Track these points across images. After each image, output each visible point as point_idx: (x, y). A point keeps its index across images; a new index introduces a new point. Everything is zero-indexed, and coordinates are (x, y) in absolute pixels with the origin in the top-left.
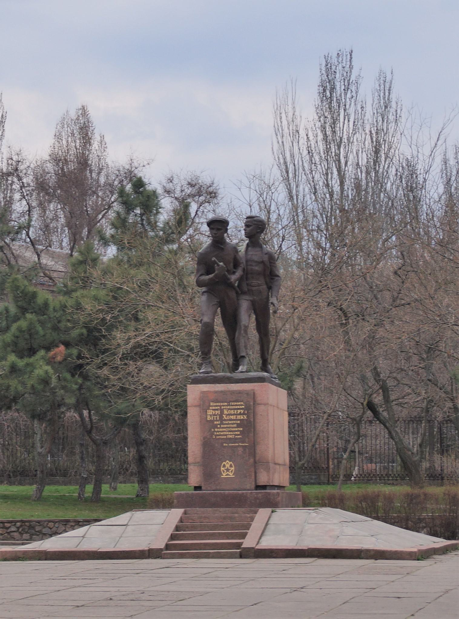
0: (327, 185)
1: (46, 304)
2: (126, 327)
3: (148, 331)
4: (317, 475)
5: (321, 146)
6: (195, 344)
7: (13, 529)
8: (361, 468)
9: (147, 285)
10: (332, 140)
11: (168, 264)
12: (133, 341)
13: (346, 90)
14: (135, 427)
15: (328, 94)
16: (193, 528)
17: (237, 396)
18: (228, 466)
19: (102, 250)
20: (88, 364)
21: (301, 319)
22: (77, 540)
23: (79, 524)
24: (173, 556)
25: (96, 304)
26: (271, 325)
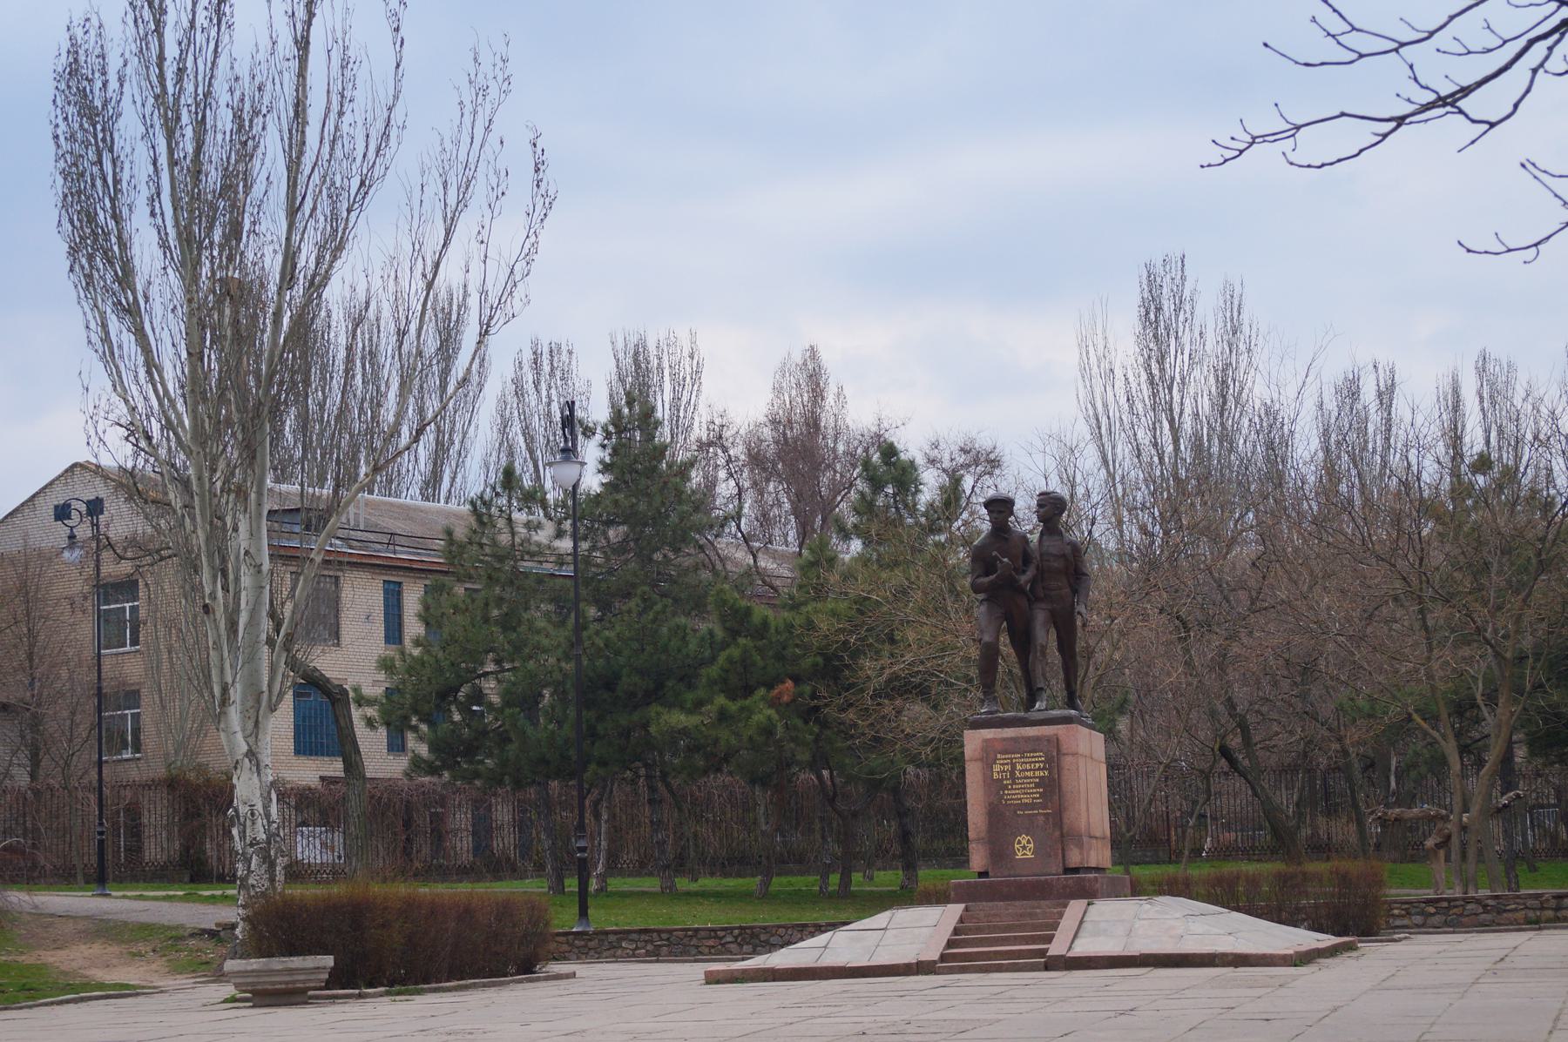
0: (1155, 445)
1: (765, 623)
2: (878, 652)
3: (909, 657)
4: (1154, 851)
5: (1146, 392)
6: (974, 672)
7: (729, 939)
8: (1216, 839)
9: (904, 592)
10: (1159, 381)
11: (934, 563)
12: (887, 671)
13: (1177, 310)
14: (895, 791)
15: (1152, 316)
16: (979, 930)
17: (1034, 744)
18: (1024, 842)
19: (842, 546)
20: (826, 705)
21: (1121, 633)
22: (817, 953)
23: (819, 929)
24: (951, 971)
25: (834, 621)
26: (1080, 645)
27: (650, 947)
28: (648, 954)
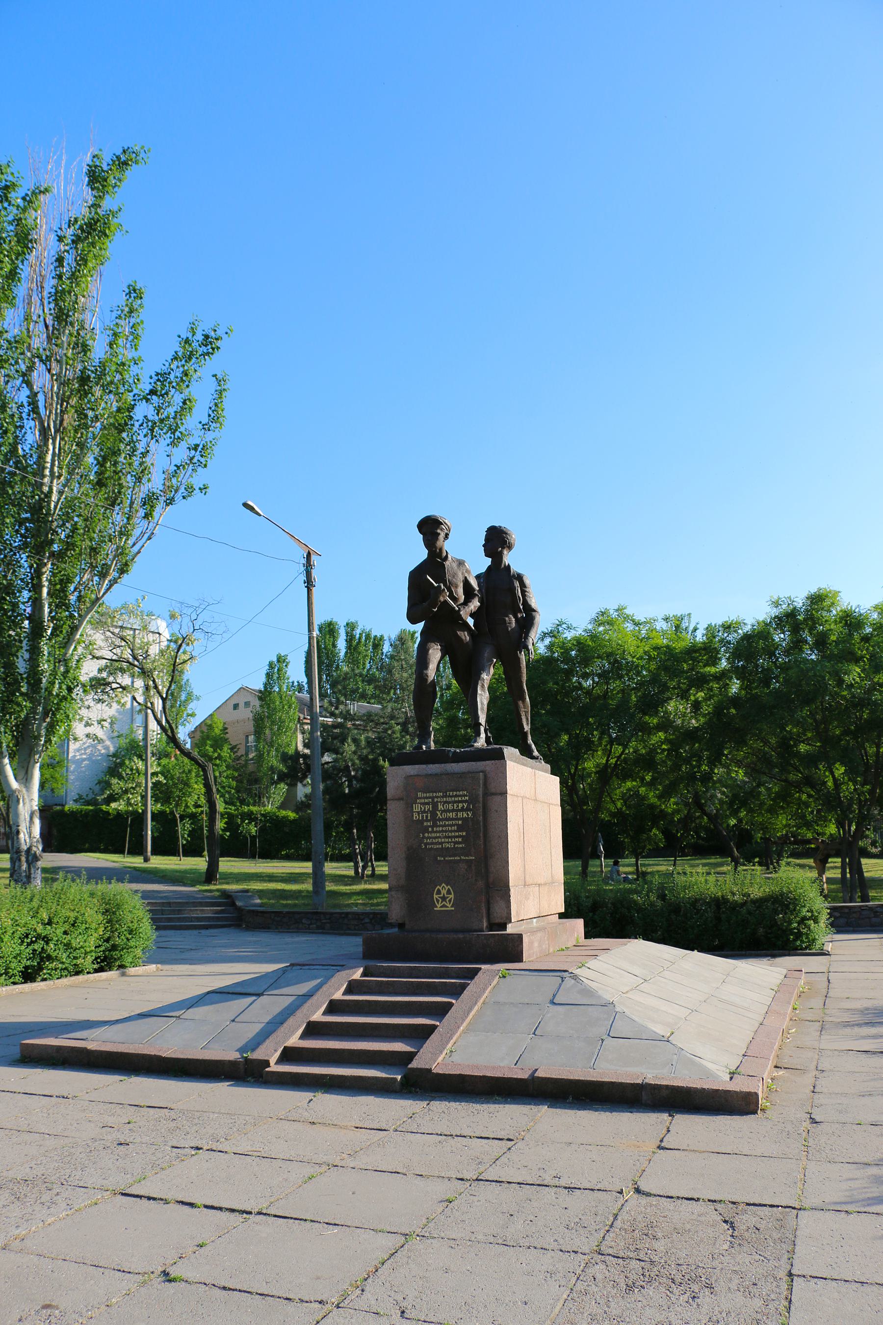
7: (367, 920)
18: (444, 892)
27: (319, 924)
28: (318, 928)
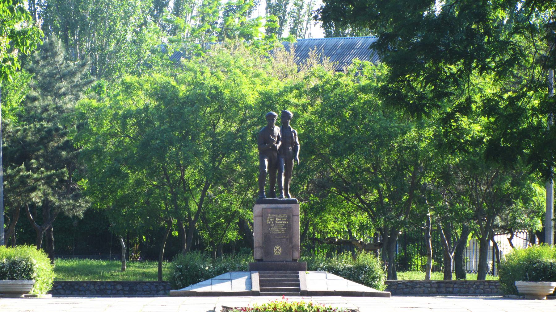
17: (284, 210)
18: (278, 248)
